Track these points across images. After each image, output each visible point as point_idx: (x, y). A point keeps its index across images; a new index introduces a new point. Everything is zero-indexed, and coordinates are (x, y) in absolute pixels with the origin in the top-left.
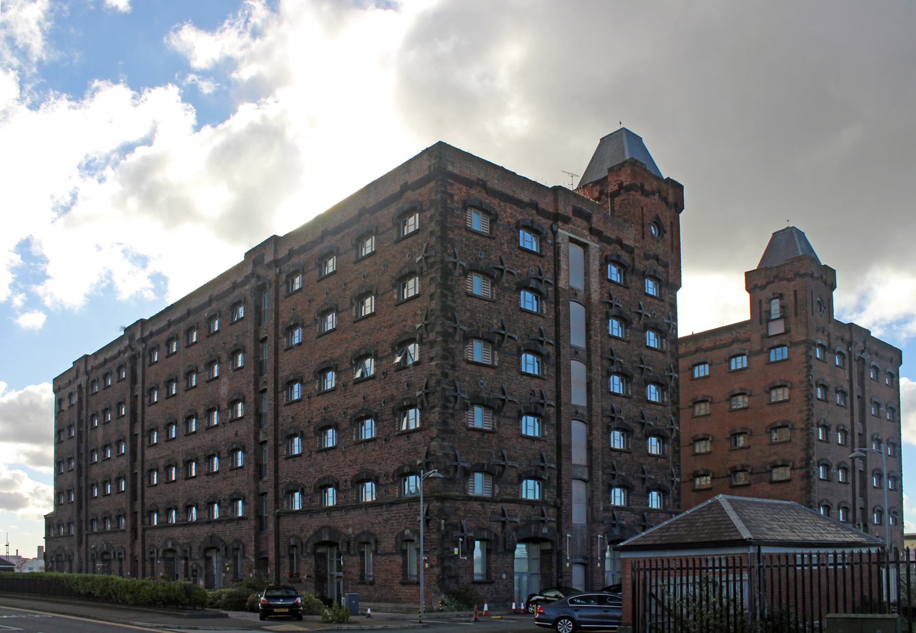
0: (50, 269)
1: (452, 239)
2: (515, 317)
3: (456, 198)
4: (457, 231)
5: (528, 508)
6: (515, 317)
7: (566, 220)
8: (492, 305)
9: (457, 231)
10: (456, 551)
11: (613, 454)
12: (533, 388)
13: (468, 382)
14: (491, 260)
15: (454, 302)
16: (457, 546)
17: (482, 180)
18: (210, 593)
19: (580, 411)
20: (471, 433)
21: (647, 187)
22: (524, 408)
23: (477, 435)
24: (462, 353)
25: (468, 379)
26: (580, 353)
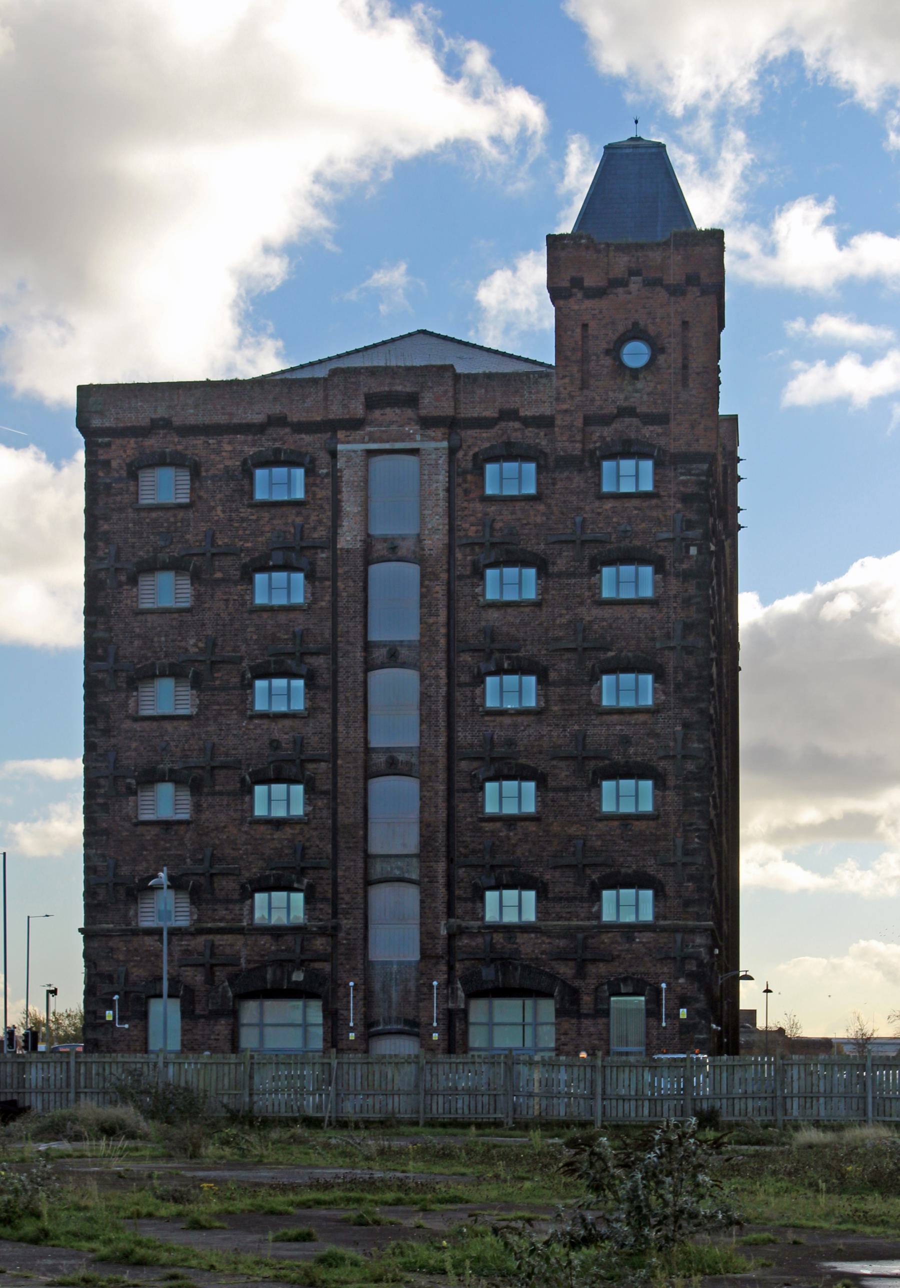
0: (303, 181)
1: (106, 533)
2: (237, 625)
3: (114, 464)
4: (115, 516)
5: (265, 941)
6: (237, 625)
7: (355, 424)
8: (188, 618)
9: (115, 516)
10: (109, 1015)
11: (487, 826)
12: (276, 735)
13: (135, 750)
14: (187, 541)
15: (110, 630)
16: (111, 1007)
17: (162, 419)
18: (393, 1243)
19: (401, 757)
20: (140, 830)
21: (589, 282)
22: (250, 774)
23: (154, 831)
24: (124, 705)
25: (134, 745)
26: (403, 652)
